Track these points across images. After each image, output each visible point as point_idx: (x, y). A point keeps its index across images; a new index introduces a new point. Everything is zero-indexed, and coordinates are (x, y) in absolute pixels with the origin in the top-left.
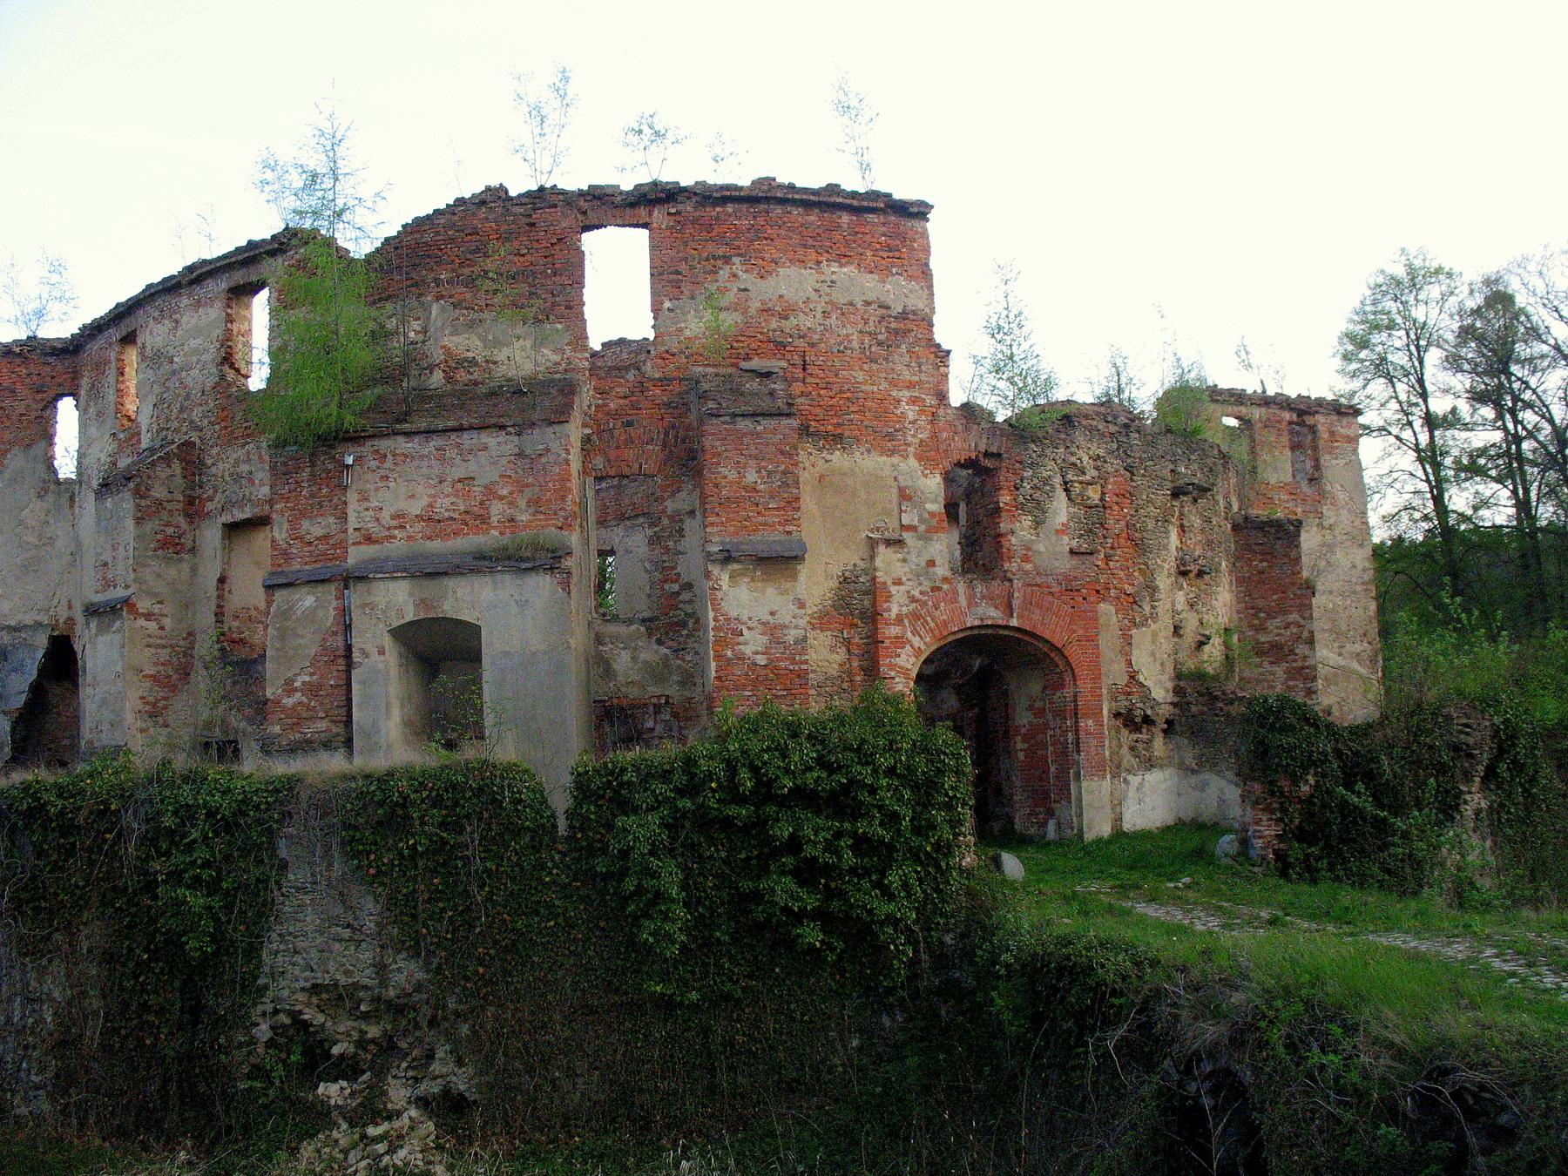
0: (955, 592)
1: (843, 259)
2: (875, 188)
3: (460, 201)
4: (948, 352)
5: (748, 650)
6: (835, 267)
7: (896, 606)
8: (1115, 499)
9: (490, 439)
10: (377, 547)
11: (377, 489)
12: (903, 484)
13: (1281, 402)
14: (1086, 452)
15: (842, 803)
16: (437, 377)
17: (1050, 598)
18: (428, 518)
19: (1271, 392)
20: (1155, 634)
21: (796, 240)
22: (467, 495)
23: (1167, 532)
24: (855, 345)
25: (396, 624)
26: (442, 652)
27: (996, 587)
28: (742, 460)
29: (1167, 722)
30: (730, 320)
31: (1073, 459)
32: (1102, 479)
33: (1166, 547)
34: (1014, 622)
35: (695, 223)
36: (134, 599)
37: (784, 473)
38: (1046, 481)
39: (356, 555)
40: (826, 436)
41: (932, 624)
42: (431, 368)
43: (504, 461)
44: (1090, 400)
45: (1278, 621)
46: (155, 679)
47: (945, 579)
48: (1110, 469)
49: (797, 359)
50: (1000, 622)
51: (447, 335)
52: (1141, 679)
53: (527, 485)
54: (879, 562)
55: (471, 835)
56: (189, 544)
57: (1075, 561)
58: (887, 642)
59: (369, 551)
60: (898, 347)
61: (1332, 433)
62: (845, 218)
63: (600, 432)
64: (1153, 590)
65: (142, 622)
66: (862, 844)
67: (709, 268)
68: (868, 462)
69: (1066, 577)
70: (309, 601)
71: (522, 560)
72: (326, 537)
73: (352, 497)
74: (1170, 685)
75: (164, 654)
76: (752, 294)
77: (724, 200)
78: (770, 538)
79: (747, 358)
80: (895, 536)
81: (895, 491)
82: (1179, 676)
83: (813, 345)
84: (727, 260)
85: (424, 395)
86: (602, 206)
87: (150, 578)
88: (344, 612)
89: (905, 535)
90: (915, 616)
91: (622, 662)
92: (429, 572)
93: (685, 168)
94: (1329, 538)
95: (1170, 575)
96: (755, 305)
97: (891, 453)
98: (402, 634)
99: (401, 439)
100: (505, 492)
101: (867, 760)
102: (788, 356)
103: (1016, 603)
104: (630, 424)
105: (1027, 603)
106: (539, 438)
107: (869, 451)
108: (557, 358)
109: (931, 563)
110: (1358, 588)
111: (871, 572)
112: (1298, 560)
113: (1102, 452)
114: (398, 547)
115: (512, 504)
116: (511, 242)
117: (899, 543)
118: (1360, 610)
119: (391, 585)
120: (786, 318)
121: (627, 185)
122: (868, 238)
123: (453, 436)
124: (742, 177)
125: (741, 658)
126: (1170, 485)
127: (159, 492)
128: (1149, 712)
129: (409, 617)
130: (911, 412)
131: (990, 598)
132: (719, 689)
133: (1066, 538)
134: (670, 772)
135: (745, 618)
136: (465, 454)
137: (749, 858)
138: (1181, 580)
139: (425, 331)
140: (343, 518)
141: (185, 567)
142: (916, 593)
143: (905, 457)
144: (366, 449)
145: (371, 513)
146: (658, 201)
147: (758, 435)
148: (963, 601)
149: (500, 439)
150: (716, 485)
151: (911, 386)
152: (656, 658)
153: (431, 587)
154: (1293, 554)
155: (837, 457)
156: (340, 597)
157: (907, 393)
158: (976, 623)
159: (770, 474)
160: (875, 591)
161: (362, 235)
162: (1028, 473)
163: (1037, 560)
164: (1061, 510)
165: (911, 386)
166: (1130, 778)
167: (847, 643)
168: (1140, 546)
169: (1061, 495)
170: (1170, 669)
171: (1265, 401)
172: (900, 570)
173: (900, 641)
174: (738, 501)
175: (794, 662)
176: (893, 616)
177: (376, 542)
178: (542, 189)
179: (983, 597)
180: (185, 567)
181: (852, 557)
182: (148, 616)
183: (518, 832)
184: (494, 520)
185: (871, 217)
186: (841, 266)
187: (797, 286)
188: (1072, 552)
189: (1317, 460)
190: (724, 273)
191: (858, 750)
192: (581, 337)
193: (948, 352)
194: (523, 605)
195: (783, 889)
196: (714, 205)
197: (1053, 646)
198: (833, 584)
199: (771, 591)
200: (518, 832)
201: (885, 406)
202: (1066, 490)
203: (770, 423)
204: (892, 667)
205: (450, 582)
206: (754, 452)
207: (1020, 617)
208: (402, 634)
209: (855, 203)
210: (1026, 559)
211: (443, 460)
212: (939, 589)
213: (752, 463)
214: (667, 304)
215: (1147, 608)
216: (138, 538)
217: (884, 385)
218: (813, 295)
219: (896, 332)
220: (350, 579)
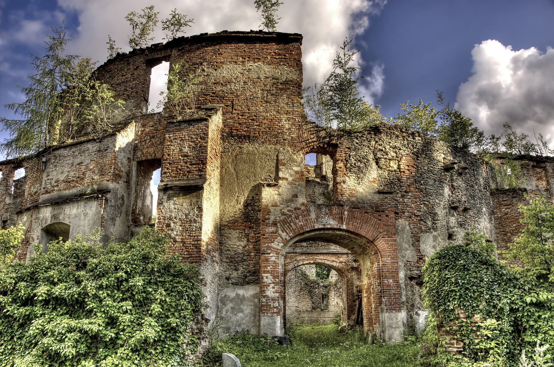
1: (254, 60)
6: (251, 63)
10: (49, 195)
11: (53, 171)
18: (66, 181)
24: (260, 95)
31: (380, 147)
33: (442, 195)
34: (344, 227)
35: (186, 49)
41: (294, 227)
49: (229, 103)
50: (335, 227)
57: (381, 196)
59: (46, 196)
60: (282, 95)
63: (141, 142)
90: (284, 222)
92: (59, 202)
104: (153, 137)
108: (130, 113)
113: (398, 145)
114: (55, 194)
121: (165, 42)
129: (49, 222)
136: (81, 153)
138: (452, 211)
140: (41, 185)
142: (285, 211)
145: (49, 181)
149: (94, 145)
151: (287, 113)
158: (321, 227)
166: (420, 312)
167: (247, 236)
169: (374, 165)
176: (271, 221)
177: (49, 193)
186: (255, 62)
202: (377, 163)
204: (269, 248)
207: (347, 224)
212: (299, 209)
215: (430, 223)
219: (281, 89)
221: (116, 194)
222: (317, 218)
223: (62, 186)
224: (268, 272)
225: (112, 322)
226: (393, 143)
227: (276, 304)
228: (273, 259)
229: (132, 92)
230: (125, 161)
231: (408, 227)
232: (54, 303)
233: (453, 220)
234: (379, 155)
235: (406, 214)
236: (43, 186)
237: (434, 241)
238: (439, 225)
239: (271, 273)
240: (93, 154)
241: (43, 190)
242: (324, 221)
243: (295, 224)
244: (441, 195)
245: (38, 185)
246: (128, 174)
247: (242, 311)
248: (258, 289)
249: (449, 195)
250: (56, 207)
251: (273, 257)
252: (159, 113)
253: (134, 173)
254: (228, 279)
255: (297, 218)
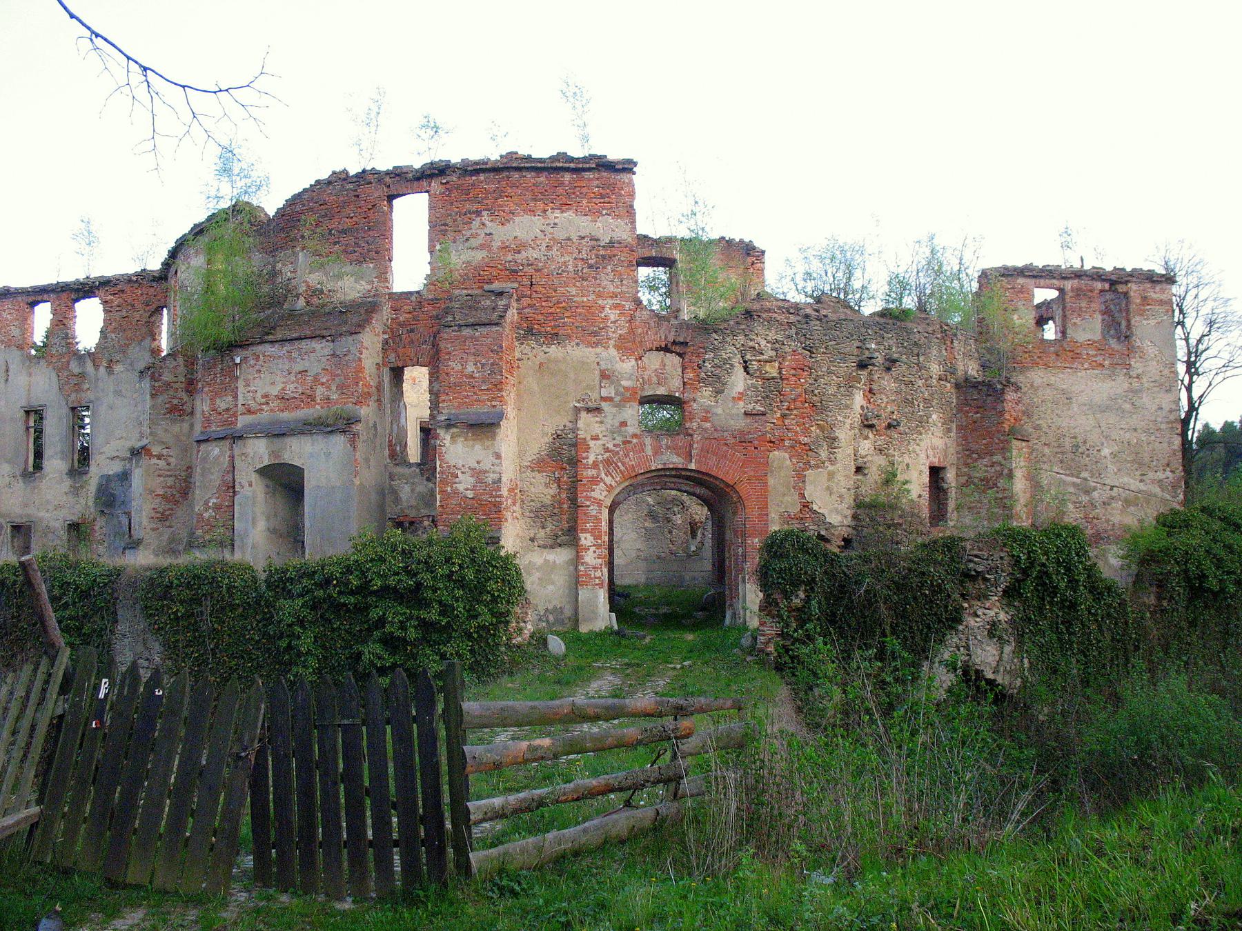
0: (642, 445)
1: (565, 206)
2: (593, 152)
3: (318, 182)
4: (763, 252)
5: (461, 487)
6: (557, 213)
7: (594, 454)
8: (793, 372)
9: (316, 345)
12: (603, 367)
13: (1097, 274)
14: (763, 337)
15: (414, 596)
16: (301, 302)
17: (725, 448)
19: (1087, 267)
20: (831, 475)
21: (529, 196)
22: (303, 383)
23: (851, 395)
24: (571, 268)
25: (258, 467)
26: (287, 483)
27: (681, 441)
28: (465, 356)
29: (844, 540)
30: (479, 256)
31: (751, 344)
32: (780, 356)
34: (692, 466)
35: (462, 188)
36: (149, 447)
37: (492, 364)
38: (725, 361)
39: (243, 421)
40: (546, 335)
41: (622, 468)
42: (298, 296)
43: (324, 359)
44: (794, 297)
45: (985, 461)
46: (164, 497)
47: (635, 436)
48: (787, 349)
51: (313, 274)
52: (815, 507)
53: (338, 375)
54: (580, 424)
55: (207, 605)
56: (189, 410)
57: (749, 420)
58: (585, 481)
59: (249, 419)
60: (604, 268)
61: (1144, 298)
62: (567, 177)
63: (393, 337)
64: (832, 441)
65: (155, 461)
66: (425, 625)
67: (466, 220)
68: (576, 352)
69: (741, 433)
70: (216, 451)
71: (328, 425)
72: (228, 410)
73: (241, 384)
74: (849, 513)
75: (170, 481)
76: (495, 237)
77: (477, 172)
78: (482, 410)
79: (490, 282)
80: (595, 405)
81: (597, 373)
82: (859, 504)
83: (537, 271)
84: (478, 213)
85: (292, 314)
86: (402, 180)
87: (160, 432)
88: (232, 457)
89: (604, 404)
90: (608, 462)
91: (405, 492)
92: (278, 433)
93: (454, 152)
94: (1136, 385)
95: (852, 428)
96: (496, 244)
97: (596, 345)
98: (264, 472)
99: (267, 345)
100: (324, 380)
101: (430, 569)
102: (519, 279)
103: (694, 452)
104: (412, 331)
105: (705, 451)
106: (347, 342)
107: (578, 344)
108: (369, 287)
109: (624, 424)
110: (1163, 426)
111: (575, 430)
112: (1002, 413)
113: (780, 338)
114: (264, 416)
115: (328, 388)
116: (348, 209)
117: (598, 410)
118: (1165, 445)
119: (256, 441)
120: (519, 252)
121: (417, 166)
122: (585, 190)
123: (296, 343)
124: (493, 153)
125: (456, 492)
126: (854, 359)
127: (167, 377)
128: (823, 533)
129: (266, 463)
130: (613, 315)
131: (674, 449)
132: (442, 513)
133: (741, 404)
134: (315, 572)
135: (460, 466)
136: (304, 354)
137: (361, 631)
138: (866, 431)
139: (295, 272)
140: (236, 397)
141: (186, 425)
142: (610, 446)
143: (606, 348)
144: (248, 353)
146: (432, 176)
147: (476, 339)
148: (649, 451)
150: (447, 374)
151: (614, 296)
152: (425, 490)
153: (278, 442)
154: (999, 408)
155: (554, 351)
156: (231, 449)
157: (610, 302)
158: (660, 467)
159: (483, 365)
160: (578, 445)
161: (271, 203)
162: (710, 356)
163: (715, 419)
164: (738, 381)
165: (614, 296)
167: (558, 481)
168: (817, 407)
169: (739, 371)
170: (849, 500)
171: (1078, 275)
172: (598, 429)
173: (595, 480)
174: (460, 384)
175: (492, 496)
176: (590, 461)
178: (364, 171)
179: (668, 448)
180: (186, 425)
181: (563, 421)
182: (159, 457)
183: (233, 608)
184: (318, 398)
185: (587, 175)
187: (526, 229)
188: (746, 414)
189: (1129, 321)
190: (476, 223)
191: (426, 563)
192: (384, 273)
193: (763, 252)
194: (328, 455)
195: (371, 651)
196: (471, 176)
197: (728, 485)
198: (549, 439)
199: (478, 447)
200: (233, 608)
201: (591, 312)
203: (484, 330)
204: (588, 498)
205: (288, 440)
206: (473, 351)
208: (264, 472)
209: (572, 165)
210: (705, 419)
211: (290, 359)
212: (630, 442)
213: (471, 358)
214: (438, 247)
216: (153, 407)
217: (593, 296)
218: (539, 234)
219: (604, 257)
220: (237, 438)
221: (367, 422)
222: (656, 453)
223: (275, 404)
224: (586, 531)
225: (445, 609)
226: (772, 335)
227: (598, 574)
228: (594, 513)
229: (369, 251)
230: (374, 370)
231: (788, 462)
232: (385, 592)
233: (866, 446)
234: (748, 357)
235: (787, 443)
236: (241, 401)
237: (829, 480)
238: (839, 456)
239: (591, 532)
240: (324, 359)
241: (241, 409)
242: (665, 458)
243: (623, 464)
244: (847, 407)
245: (230, 398)
246: (379, 388)
247: (553, 583)
248: (574, 553)
249: (862, 407)
250: (276, 440)
251: (593, 509)
252: (418, 292)
253: (387, 385)
254: (532, 540)
255: (626, 456)
